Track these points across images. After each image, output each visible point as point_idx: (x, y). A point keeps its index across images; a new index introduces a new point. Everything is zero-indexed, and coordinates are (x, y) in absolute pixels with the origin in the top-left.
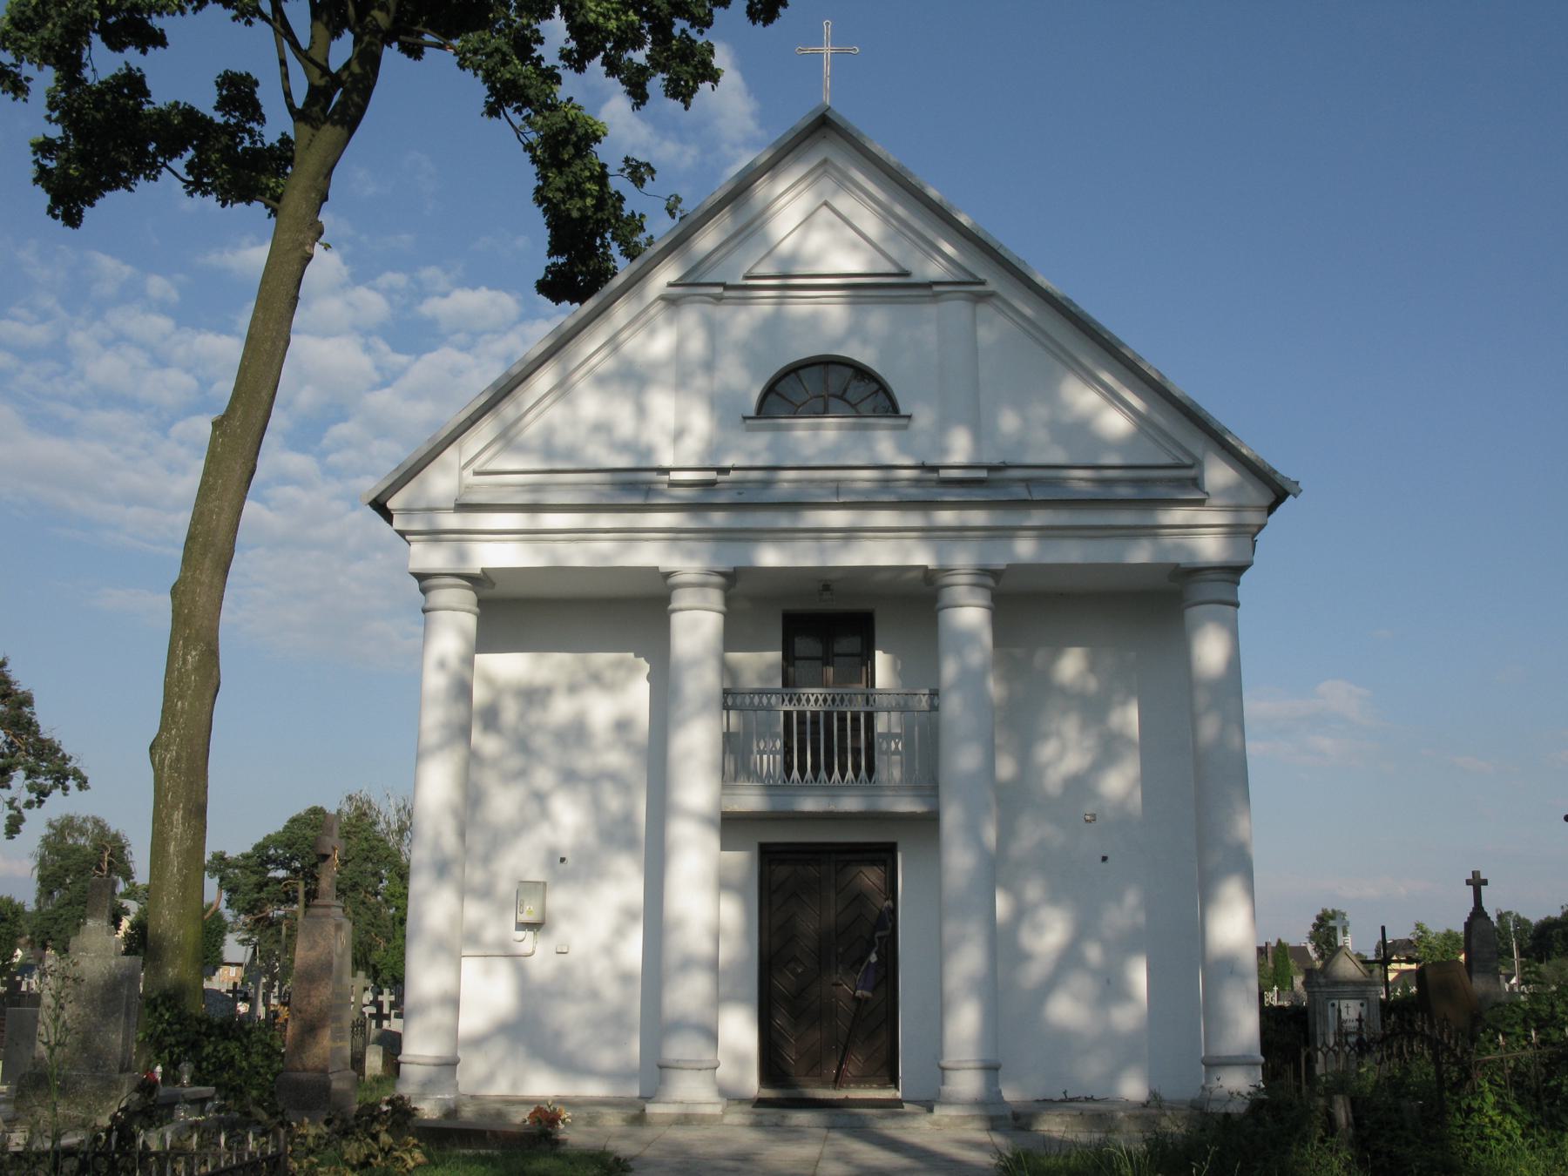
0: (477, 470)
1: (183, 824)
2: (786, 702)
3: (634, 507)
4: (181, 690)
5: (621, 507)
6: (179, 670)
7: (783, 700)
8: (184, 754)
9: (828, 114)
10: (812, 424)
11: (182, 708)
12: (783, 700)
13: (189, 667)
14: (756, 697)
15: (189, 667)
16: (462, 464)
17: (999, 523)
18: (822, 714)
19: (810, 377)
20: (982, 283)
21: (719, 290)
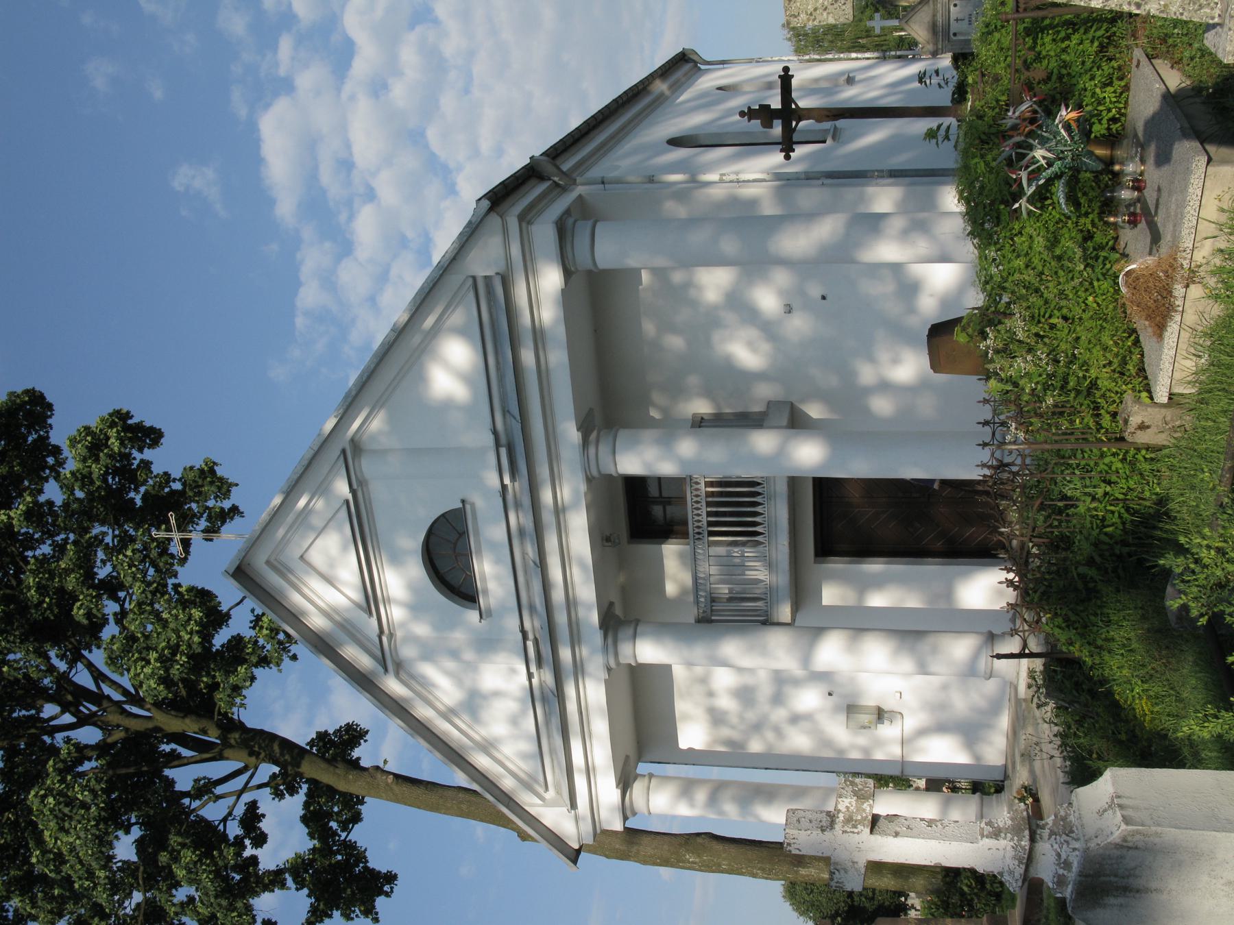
0: (544, 789)
1: (808, 867)
2: (698, 486)
3: (562, 710)
4: (714, 865)
5: (562, 710)
6: (700, 866)
7: (699, 539)
8: (759, 865)
9: (231, 572)
10: (474, 536)
11: (727, 865)
12: (699, 539)
13: (697, 860)
14: (701, 593)
15: (697, 860)
16: (540, 802)
17: (531, 344)
18: (709, 509)
19: (443, 567)
20: (344, 452)
21: (385, 639)
